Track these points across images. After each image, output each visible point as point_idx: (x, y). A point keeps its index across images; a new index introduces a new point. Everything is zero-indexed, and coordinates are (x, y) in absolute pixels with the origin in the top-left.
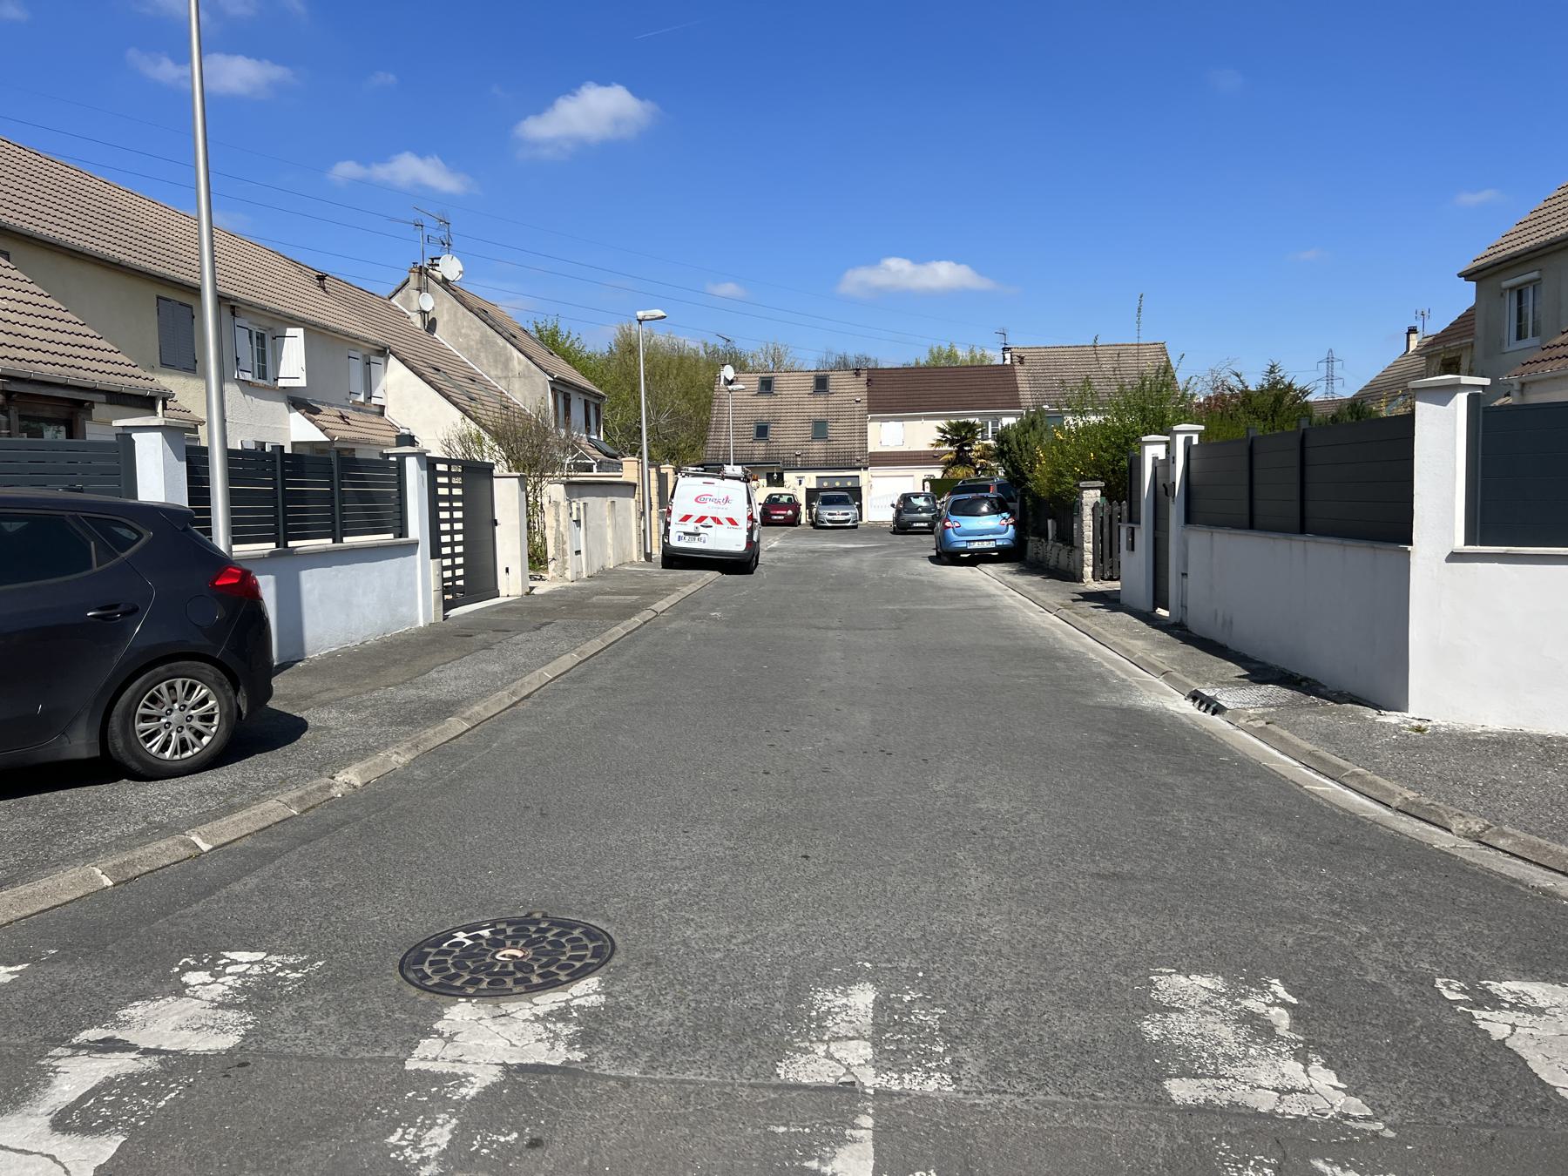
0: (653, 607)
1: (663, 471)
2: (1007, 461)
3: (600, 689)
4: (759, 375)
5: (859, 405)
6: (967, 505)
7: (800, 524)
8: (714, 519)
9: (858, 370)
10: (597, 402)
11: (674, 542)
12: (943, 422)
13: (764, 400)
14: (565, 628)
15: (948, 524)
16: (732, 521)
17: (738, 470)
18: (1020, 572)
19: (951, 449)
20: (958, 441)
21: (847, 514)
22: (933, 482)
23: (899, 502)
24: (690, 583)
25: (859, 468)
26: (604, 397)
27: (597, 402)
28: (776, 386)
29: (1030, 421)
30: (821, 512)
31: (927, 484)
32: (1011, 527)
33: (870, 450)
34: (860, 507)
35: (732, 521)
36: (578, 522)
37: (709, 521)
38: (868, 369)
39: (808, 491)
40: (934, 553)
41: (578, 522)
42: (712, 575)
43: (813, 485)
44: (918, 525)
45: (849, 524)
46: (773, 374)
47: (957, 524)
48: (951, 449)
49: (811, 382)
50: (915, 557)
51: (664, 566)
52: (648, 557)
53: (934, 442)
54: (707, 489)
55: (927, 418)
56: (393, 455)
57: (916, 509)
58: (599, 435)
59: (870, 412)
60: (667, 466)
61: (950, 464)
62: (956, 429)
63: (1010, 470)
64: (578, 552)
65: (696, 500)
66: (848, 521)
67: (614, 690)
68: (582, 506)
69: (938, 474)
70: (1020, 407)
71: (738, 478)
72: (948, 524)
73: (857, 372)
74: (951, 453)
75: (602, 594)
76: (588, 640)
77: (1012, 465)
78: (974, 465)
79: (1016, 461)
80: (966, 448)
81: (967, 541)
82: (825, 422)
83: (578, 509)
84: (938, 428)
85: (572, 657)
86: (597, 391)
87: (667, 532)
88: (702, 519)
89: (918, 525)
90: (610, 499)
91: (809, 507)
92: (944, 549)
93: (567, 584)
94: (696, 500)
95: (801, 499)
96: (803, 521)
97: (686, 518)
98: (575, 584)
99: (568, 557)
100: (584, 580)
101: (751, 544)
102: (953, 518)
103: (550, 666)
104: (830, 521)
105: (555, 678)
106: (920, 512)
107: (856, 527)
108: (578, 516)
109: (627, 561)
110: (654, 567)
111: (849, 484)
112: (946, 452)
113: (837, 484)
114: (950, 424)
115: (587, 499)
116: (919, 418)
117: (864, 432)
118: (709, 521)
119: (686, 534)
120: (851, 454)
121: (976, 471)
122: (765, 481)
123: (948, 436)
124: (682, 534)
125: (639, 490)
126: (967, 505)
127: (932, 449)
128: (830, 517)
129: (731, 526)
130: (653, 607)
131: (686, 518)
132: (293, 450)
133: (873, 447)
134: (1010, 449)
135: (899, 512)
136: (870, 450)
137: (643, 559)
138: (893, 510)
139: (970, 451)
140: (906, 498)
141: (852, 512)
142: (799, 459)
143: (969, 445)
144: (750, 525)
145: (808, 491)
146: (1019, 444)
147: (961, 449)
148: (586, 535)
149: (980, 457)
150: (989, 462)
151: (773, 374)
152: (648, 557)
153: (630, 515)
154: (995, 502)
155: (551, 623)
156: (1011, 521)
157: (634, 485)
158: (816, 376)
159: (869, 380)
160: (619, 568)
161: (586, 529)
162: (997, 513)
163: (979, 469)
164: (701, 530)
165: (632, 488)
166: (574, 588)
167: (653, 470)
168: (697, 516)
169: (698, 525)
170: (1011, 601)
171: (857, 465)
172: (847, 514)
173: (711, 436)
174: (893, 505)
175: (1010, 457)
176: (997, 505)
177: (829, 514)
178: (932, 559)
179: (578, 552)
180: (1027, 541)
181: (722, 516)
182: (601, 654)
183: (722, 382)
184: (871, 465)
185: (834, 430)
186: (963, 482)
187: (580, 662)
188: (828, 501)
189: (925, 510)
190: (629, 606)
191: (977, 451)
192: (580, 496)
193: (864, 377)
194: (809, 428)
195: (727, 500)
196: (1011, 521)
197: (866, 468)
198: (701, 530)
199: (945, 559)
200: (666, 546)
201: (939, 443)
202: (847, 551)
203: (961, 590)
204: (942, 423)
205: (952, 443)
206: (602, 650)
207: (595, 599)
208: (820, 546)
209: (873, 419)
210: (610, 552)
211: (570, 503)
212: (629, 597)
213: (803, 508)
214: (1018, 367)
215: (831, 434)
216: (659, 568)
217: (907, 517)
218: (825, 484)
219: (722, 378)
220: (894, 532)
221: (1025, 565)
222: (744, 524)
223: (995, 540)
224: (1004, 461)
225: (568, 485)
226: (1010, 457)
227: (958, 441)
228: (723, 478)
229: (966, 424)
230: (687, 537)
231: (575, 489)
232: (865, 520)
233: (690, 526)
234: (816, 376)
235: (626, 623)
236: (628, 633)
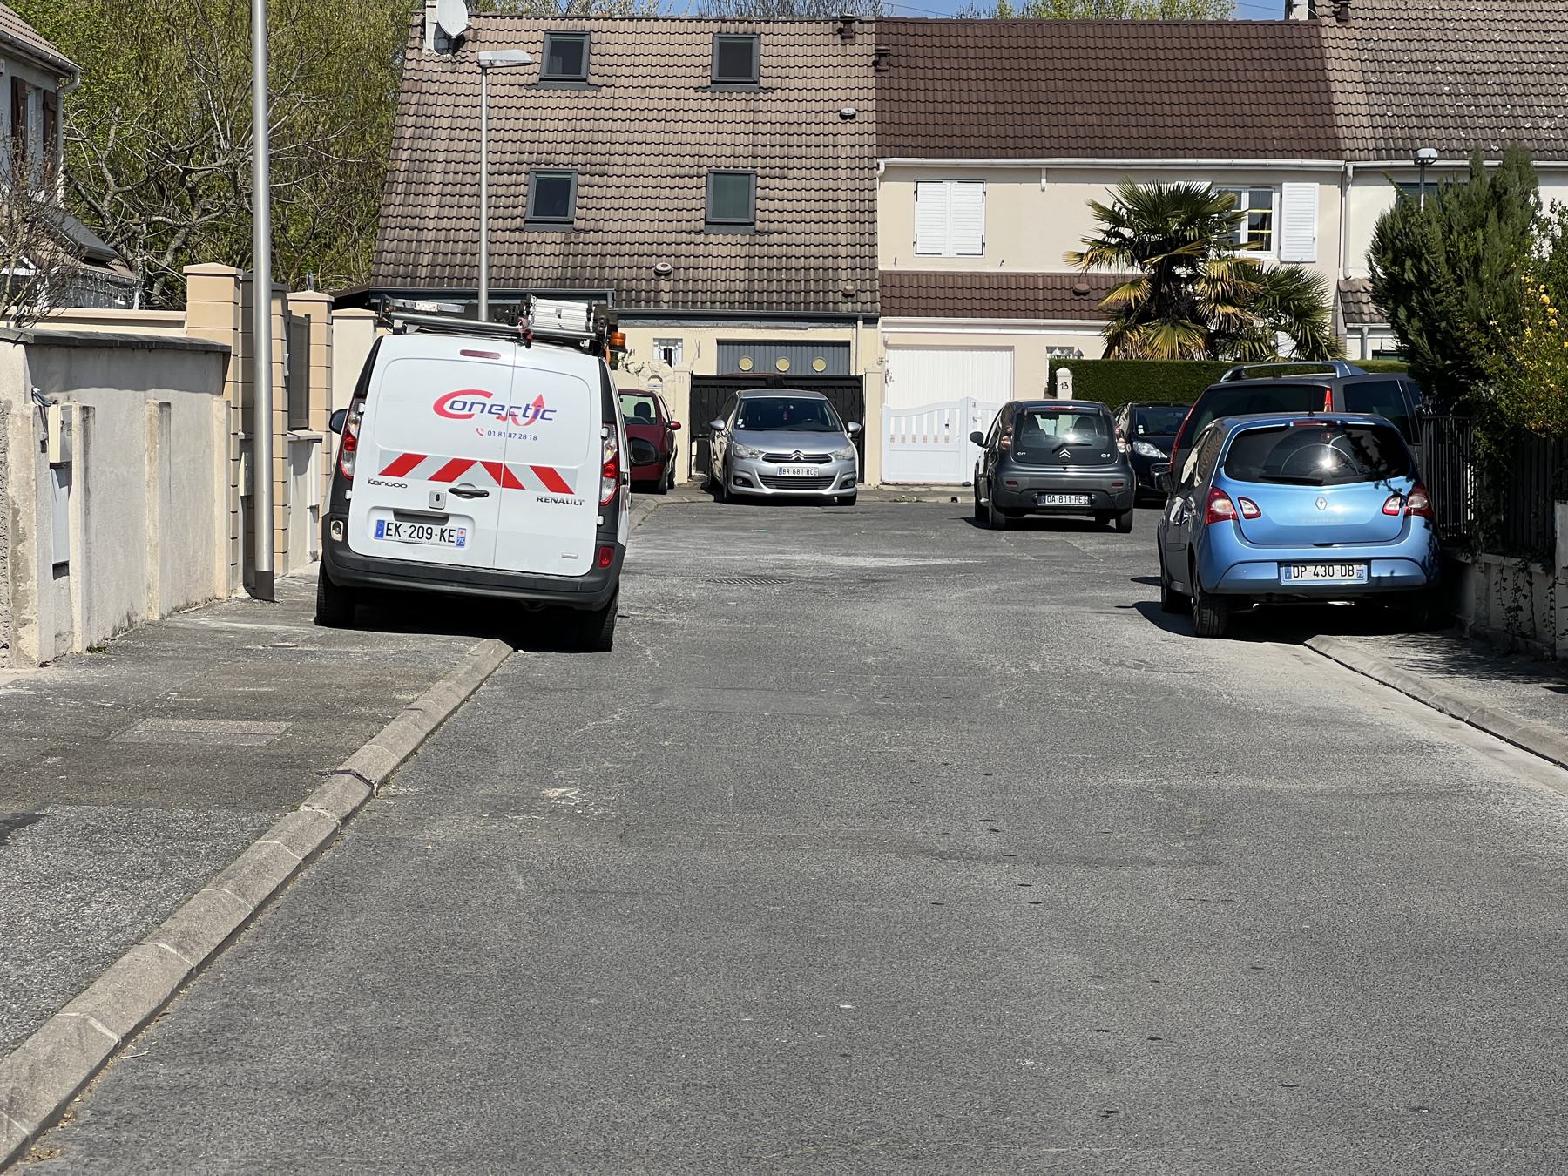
0: (353, 763)
1: (298, 310)
2: (1411, 313)
3: (307, 1087)
4: (545, 24)
5: (850, 128)
6: (1283, 444)
7: (672, 486)
8: (494, 469)
9: (848, 21)
10: (48, 85)
11: (363, 540)
12: (1114, 188)
13: (558, 103)
14: (89, 838)
15: (1219, 506)
16: (552, 479)
17: (574, 316)
18: (1459, 666)
19: (1136, 270)
20: (1158, 248)
21: (824, 459)
22: (1081, 369)
23: (999, 433)
24: (432, 678)
25: (850, 320)
26: (70, 73)
27: (48, 85)
28: (596, 61)
29: (1485, 193)
30: (742, 450)
31: (1064, 374)
32: (1417, 522)
33: (884, 265)
34: (859, 438)
35: (552, 479)
36: (62, 469)
37: (477, 478)
38: (879, 20)
39: (698, 383)
40: (1154, 595)
41: (62, 469)
42: (487, 653)
43: (709, 367)
44: (1056, 500)
45: (826, 492)
46: (588, 25)
47: (1248, 509)
48: (1136, 270)
49: (704, 54)
50: (1096, 604)
51: (321, 620)
52: (260, 585)
53: (1085, 248)
54: (473, 374)
55: (1055, 174)
56: (120, 307)
57: (1052, 454)
58: (51, 193)
59: (884, 149)
60: (310, 294)
61: (1132, 316)
62: (1151, 210)
63: (1423, 342)
64: (61, 569)
65: (438, 408)
66: (826, 480)
67: (362, 1094)
68: (76, 417)
69: (1091, 345)
70: (1337, 153)
71: (571, 342)
72: (1219, 506)
73: (846, 28)
74: (1136, 283)
75: (163, 713)
76: (191, 888)
77: (1430, 330)
78: (1202, 321)
79: (1445, 315)
80: (1181, 272)
81: (1281, 563)
82: (745, 177)
83: (66, 425)
84: (1094, 205)
85: (162, 954)
86: (52, 52)
87: (339, 510)
88: (454, 469)
89: (1056, 500)
90: (155, 396)
91: (701, 431)
92: (1208, 586)
93: (29, 673)
94: (438, 408)
95: (678, 408)
96: (681, 477)
97: (404, 465)
98: (54, 675)
99: (31, 585)
100: (77, 660)
101: (608, 551)
102: (1234, 487)
103: (103, 990)
104: (768, 479)
105: (127, 1039)
106: (1064, 463)
107: (848, 500)
108: (65, 449)
109: (197, 597)
110: (288, 619)
111: (819, 366)
112: (1120, 282)
113: (783, 366)
114: (1133, 196)
115: (89, 396)
116: (1031, 174)
117: (865, 214)
118: (477, 478)
119: (400, 514)
120: (828, 275)
121: (1210, 339)
122: (712, 371)
123: (1127, 232)
124: (389, 517)
125: (235, 369)
126: (1283, 444)
127: (1077, 269)
128: (771, 468)
129: (547, 493)
130: (353, 763)
131: (404, 465)
132: (718, 372)
133: (892, 257)
134: (1424, 279)
135: (997, 458)
136: (884, 265)
137: (242, 593)
138: (978, 452)
139: (1193, 279)
140: (1019, 417)
141: (839, 453)
142: (664, 285)
143: (1190, 261)
144: (608, 492)
145: (698, 383)
146: (1451, 261)
147: (1163, 275)
148: (87, 512)
149: (1225, 300)
150: (1248, 315)
151: (588, 25)
152: (260, 585)
153: (209, 445)
154: (1368, 441)
155: (33, 819)
156: (1417, 502)
157: (224, 354)
158: (718, 35)
159: (880, 54)
160: (179, 621)
161: (87, 491)
162: (1376, 476)
163: (1217, 333)
164: (453, 505)
165: (214, 363)
166: (61, 691)
167: (277, 305)
168: (440, 456)
169: (443, 487)
170: (1500, 768)
171: (846, 308)
172: (824, 459)
173: (394, 206)
174: (977, 438)
175: (1424, 304)
176: (1374, 453)
177: (769, 458)
178: (1147, 610)
179: (61, 569)
180: (1463, 567)
181: (518, 461)
182: (243, 939)
183: (429, 43)
184: (890, 311)
185: (768, 205)
186: (1236, 376)
187: (190, 975)
188: (762, 419)
189: (1081, 456)
190: (270, 760)
191: (1212, 281)
192: (69, 385)
193: (865, 44)
194: (695, 194)
195: (538, 410)
196: (1417, 502)
197: (871, 321)
198: (453, 505)
199: (1209, 616)
200: (334, 555)
201: (1099, 250)
202: (871, 581)
203: (1308, 721)
204: (1109, 194)
205: (1138, 252)
206: (244, 925)
207: (144, 730)
208: (773, 558)
209: (892, 173)
210: (151, 568)
211: (43, 408)
212: (256, 727)
213: (682, 438)
214: (1331, 31)
215: (764, 211)
216: (304, 630)
217: (1025, 474)
218: (746, 365)
219: (430, 31)
220: (981, 519)
221: (1462, 641)
222: (590, 489)
223: (1366, 561)
224: (1402, 313)
225: (39, 347)
226: (1424, 304)
227: (1158, 248)
228: (527, 339)
229: (1185, 199)
230: (406, 527)
231: (57, 362)
232: (872, 479)
233: (417, 492)
234: (718, 35)
235: (290, 823)
236: (308, 860)
